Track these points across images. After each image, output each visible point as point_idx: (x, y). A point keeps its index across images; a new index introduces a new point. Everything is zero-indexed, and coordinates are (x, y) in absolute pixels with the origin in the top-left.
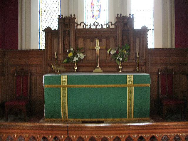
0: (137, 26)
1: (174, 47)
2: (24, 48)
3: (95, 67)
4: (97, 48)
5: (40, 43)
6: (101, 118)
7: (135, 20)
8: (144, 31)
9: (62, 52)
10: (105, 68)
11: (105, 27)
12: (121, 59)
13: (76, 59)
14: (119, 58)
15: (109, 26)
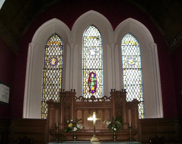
1: (160, 115)
8: (135, 102)
9: (62, 122)
10: (124, 121)
12: (115, 129)
14: (113, 128)
15: (104, 99)
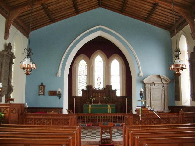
0: (113, 89)
2: (74, 96)
3: (99, 103)
4: (100, 96)
5: (80, 94)
6: (24, 124)
7: (112, 87)
8: (116, 90)
11: (102, 89)
13: (93, 100)
